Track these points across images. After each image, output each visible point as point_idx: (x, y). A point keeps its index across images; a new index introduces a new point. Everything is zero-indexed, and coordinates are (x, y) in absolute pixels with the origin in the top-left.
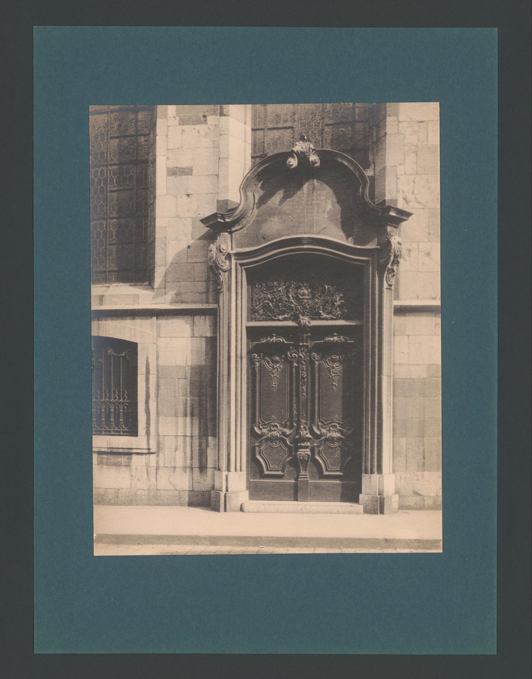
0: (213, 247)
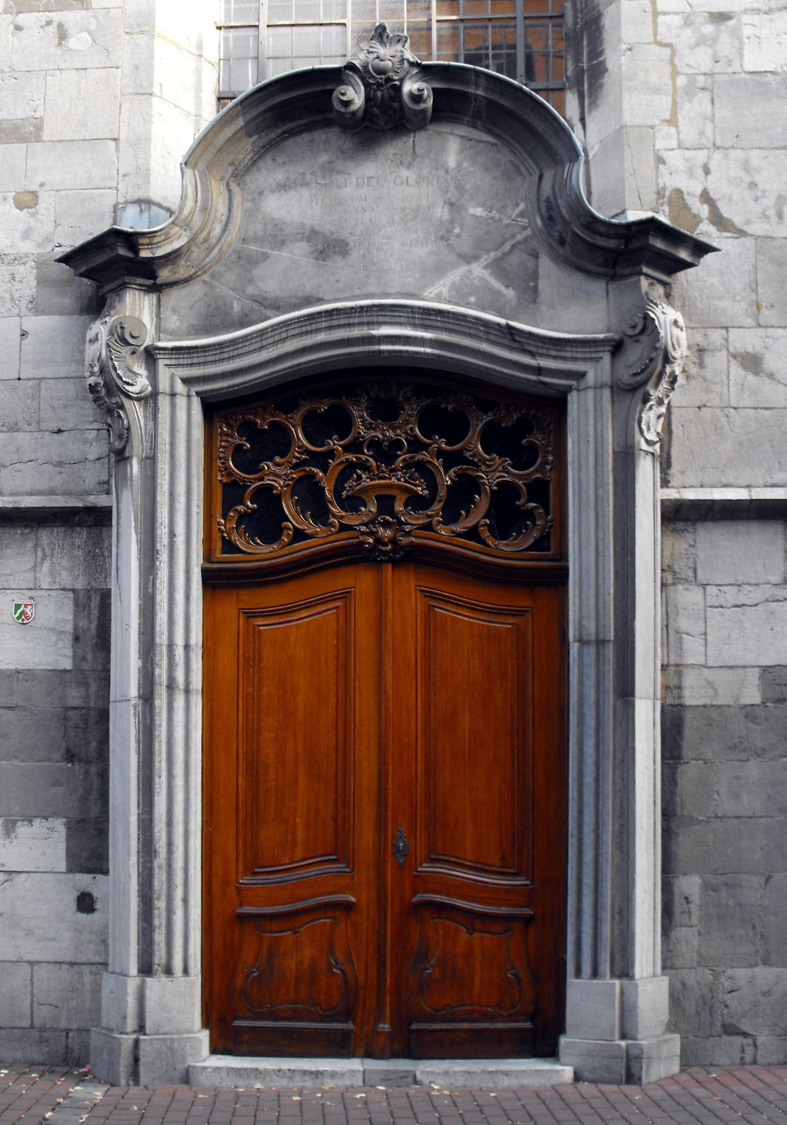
0: (100, 329)
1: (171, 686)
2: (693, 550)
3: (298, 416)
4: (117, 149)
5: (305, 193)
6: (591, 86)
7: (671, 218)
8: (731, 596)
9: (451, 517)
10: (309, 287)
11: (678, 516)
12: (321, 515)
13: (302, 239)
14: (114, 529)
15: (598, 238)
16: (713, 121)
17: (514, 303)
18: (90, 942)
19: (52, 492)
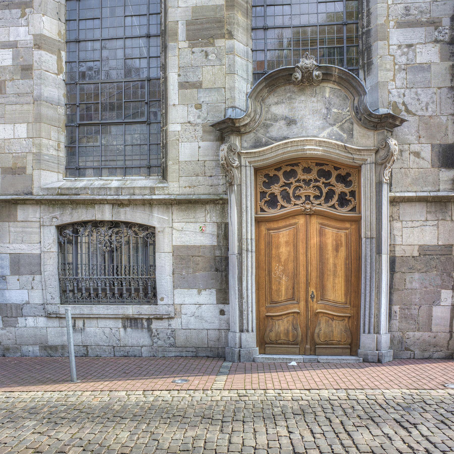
0: (224, 147)
1: (247, 251)
4: (225, 91)
6: (367, 69)
7: (393, 111)
8: (410, 224)
11: (394, 201)
12: (289, 201)
13: (283, 120)
17: (346, 138)
18: (224, 323)
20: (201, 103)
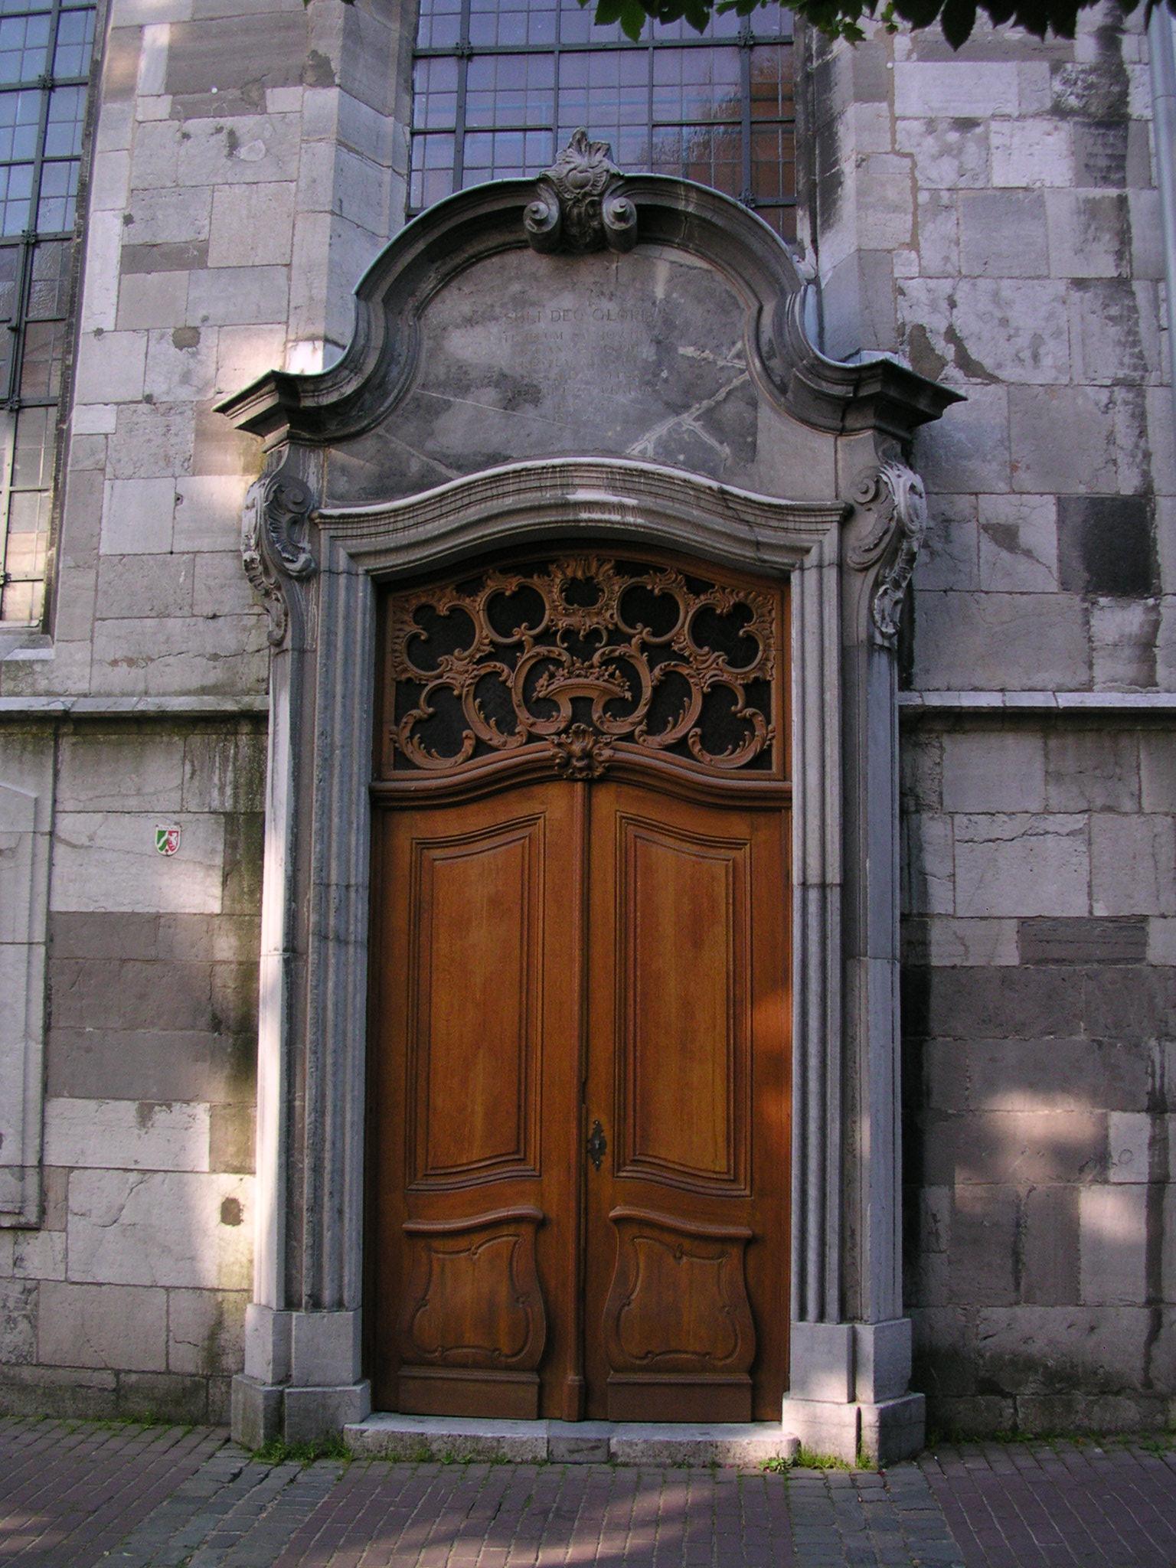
2: (938, 770)
3: (481, 600)
5: (494, 328)
7: (913, 360)
9: (655, 723)
10: (495, 440)
12: (507, 725)
14: (270, 737)
15: (824, 384)
16: (958, 244)
17: (729, 463)
19: (204, 691)
20: (197, 323)
